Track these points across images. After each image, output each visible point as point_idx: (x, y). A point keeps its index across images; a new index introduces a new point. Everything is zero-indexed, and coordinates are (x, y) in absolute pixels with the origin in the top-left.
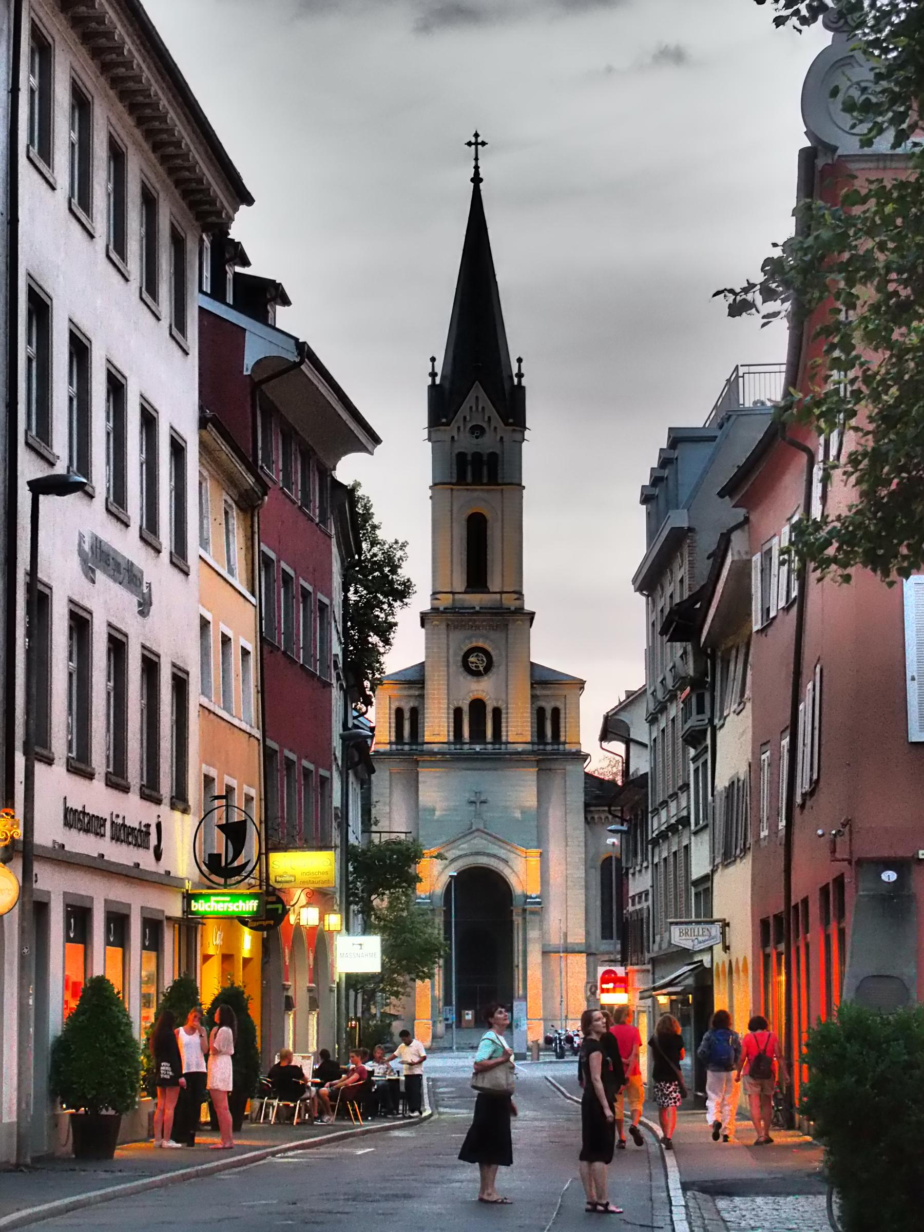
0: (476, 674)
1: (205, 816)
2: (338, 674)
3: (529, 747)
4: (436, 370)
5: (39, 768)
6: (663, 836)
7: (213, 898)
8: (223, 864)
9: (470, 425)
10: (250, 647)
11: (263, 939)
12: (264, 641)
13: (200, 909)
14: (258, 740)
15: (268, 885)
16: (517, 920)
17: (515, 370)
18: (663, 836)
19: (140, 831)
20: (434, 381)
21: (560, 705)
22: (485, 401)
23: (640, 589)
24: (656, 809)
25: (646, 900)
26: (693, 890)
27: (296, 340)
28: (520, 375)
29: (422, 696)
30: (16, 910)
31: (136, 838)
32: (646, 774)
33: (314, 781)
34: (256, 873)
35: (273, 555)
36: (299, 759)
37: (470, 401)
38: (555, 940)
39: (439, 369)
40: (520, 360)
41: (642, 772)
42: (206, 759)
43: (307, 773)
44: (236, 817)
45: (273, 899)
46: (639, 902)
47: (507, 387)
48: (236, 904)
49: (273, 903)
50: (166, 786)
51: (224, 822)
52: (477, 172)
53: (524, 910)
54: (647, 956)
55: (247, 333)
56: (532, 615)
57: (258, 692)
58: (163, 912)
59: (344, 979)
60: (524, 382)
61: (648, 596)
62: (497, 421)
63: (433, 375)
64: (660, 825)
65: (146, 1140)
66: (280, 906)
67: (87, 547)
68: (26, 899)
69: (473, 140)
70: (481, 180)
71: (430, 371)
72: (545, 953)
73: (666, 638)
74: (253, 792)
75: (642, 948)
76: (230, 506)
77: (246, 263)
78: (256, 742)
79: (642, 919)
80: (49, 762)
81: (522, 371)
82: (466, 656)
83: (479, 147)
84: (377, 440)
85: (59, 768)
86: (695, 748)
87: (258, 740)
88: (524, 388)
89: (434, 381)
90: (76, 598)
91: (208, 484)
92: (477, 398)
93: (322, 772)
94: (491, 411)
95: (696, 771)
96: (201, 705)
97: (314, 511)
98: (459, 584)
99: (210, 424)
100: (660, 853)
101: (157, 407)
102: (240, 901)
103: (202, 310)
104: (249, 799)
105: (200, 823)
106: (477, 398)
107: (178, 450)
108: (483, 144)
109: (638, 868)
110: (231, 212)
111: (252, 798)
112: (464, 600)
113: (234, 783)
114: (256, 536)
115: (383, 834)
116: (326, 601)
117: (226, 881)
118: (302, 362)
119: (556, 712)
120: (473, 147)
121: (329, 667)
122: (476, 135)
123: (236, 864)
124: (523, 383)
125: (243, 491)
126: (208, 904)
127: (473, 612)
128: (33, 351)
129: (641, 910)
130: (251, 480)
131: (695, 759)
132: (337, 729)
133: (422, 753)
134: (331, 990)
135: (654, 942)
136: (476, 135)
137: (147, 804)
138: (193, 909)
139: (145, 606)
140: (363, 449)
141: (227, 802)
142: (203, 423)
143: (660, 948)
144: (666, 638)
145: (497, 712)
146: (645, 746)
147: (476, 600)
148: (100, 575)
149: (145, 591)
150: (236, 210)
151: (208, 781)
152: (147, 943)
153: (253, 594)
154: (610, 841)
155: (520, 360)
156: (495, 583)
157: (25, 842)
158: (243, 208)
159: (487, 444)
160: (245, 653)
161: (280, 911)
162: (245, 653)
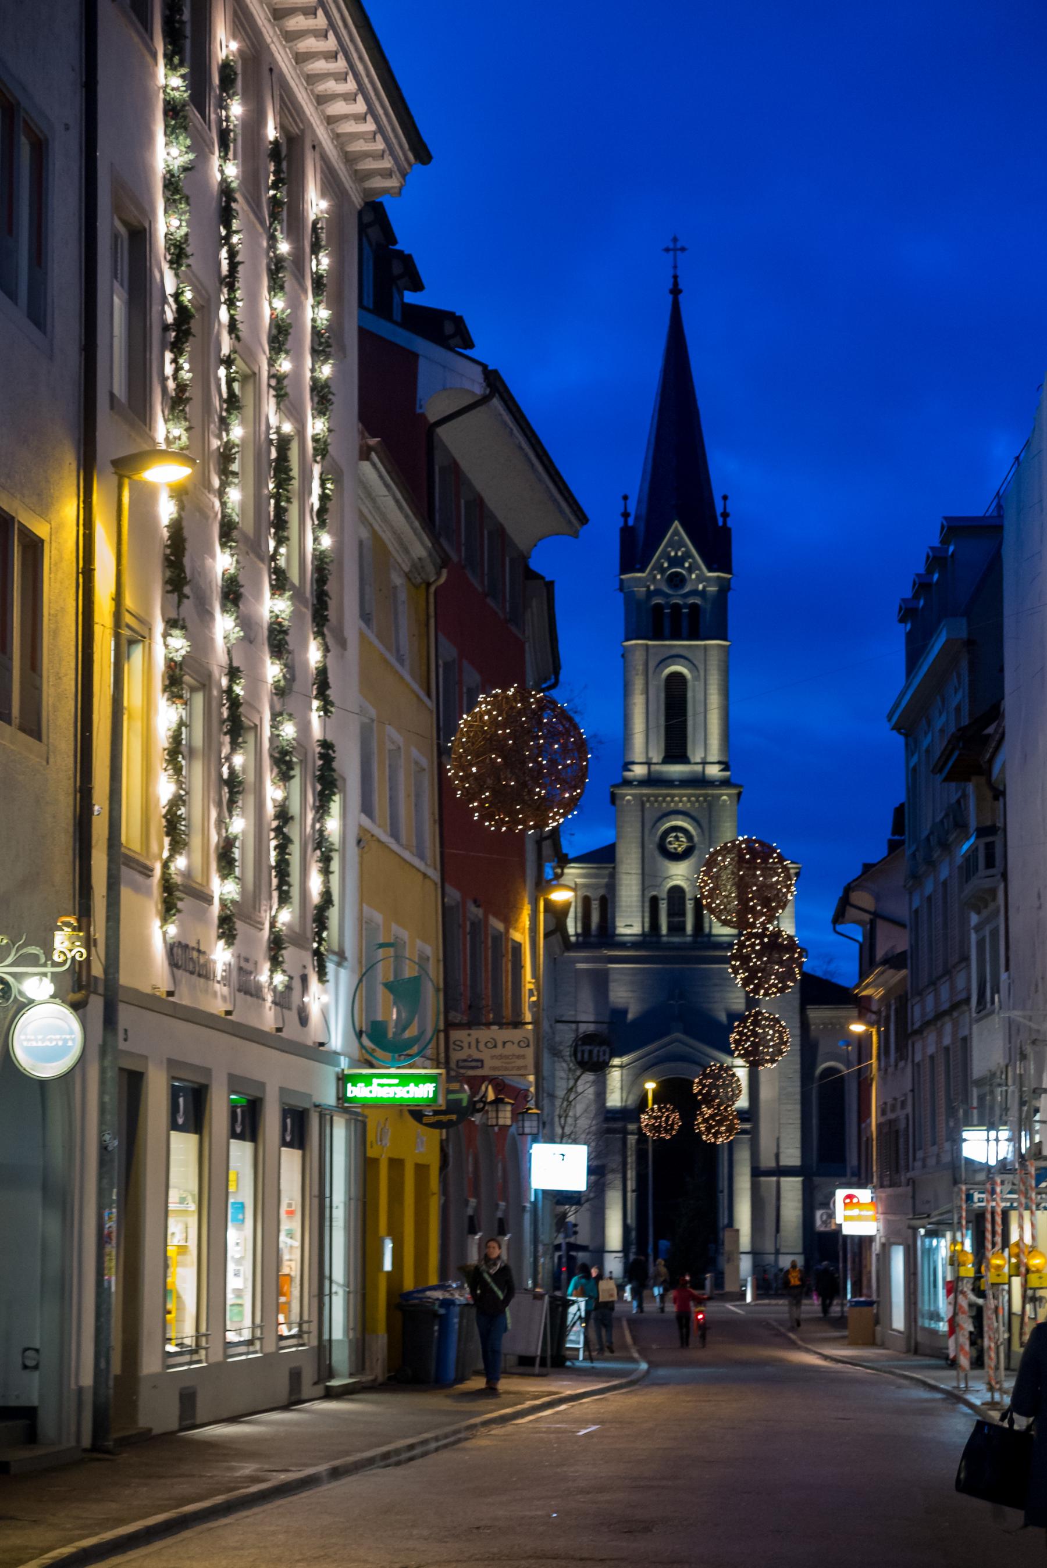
1: (367, 971)
4: (629, 510)
7: (375, 1081)
11: (442, 1141)
13: (359, 1096)
14: (436, 884)
17: (719, 509)
20: (626, 521)
23: (897, 728)
27: (484, 367)
28: (725, 515)
32: (904, 953)
38: (767, 1161)
39: (632, 508)
40: (725, 498)
41: (899, 950)
48: (407, 1088)
51: (392, 979)
52: (676, 283)
55: (422, 362)
57: (435, 821)
58: (310, 1096)
59: (540, 1196)
60: (730, 523)
61: (906, 736)
63: (626, 515)
65: (286, 1407)
68: (107, 1063)
69: (671, 246)
70: (680, 291)
71: (622, 510)
72: (757, 1172)
73: (940, 778)
77: (417, 286)
79: (897, 1132)
81: (728, 510)
83: (679, 253)
86: (979, 913)
87: (436, 884)
88: (729, 530)
89: (626, 521)
95: (981, 944)
100: (924, 1048)
102: (412, 1085)
105: (360, 981)
108: (683, 249)
111: (428, 959)
112: (661, 773)
114: (432, 621)
115: (581, 1025)
120: (671, 253)
122: (675, 240)
124: (729, 524)
125: (416, 560)
126: (369, 1088)
131: (978, 928)
135: (914, 1159)
136: (675, 240)
138: (349, 1095)
141: (396, 952)
144: (940, 778)
152: (288, 1139)
153: (429, 695)
155: (725, 498)
157: (106, 980)
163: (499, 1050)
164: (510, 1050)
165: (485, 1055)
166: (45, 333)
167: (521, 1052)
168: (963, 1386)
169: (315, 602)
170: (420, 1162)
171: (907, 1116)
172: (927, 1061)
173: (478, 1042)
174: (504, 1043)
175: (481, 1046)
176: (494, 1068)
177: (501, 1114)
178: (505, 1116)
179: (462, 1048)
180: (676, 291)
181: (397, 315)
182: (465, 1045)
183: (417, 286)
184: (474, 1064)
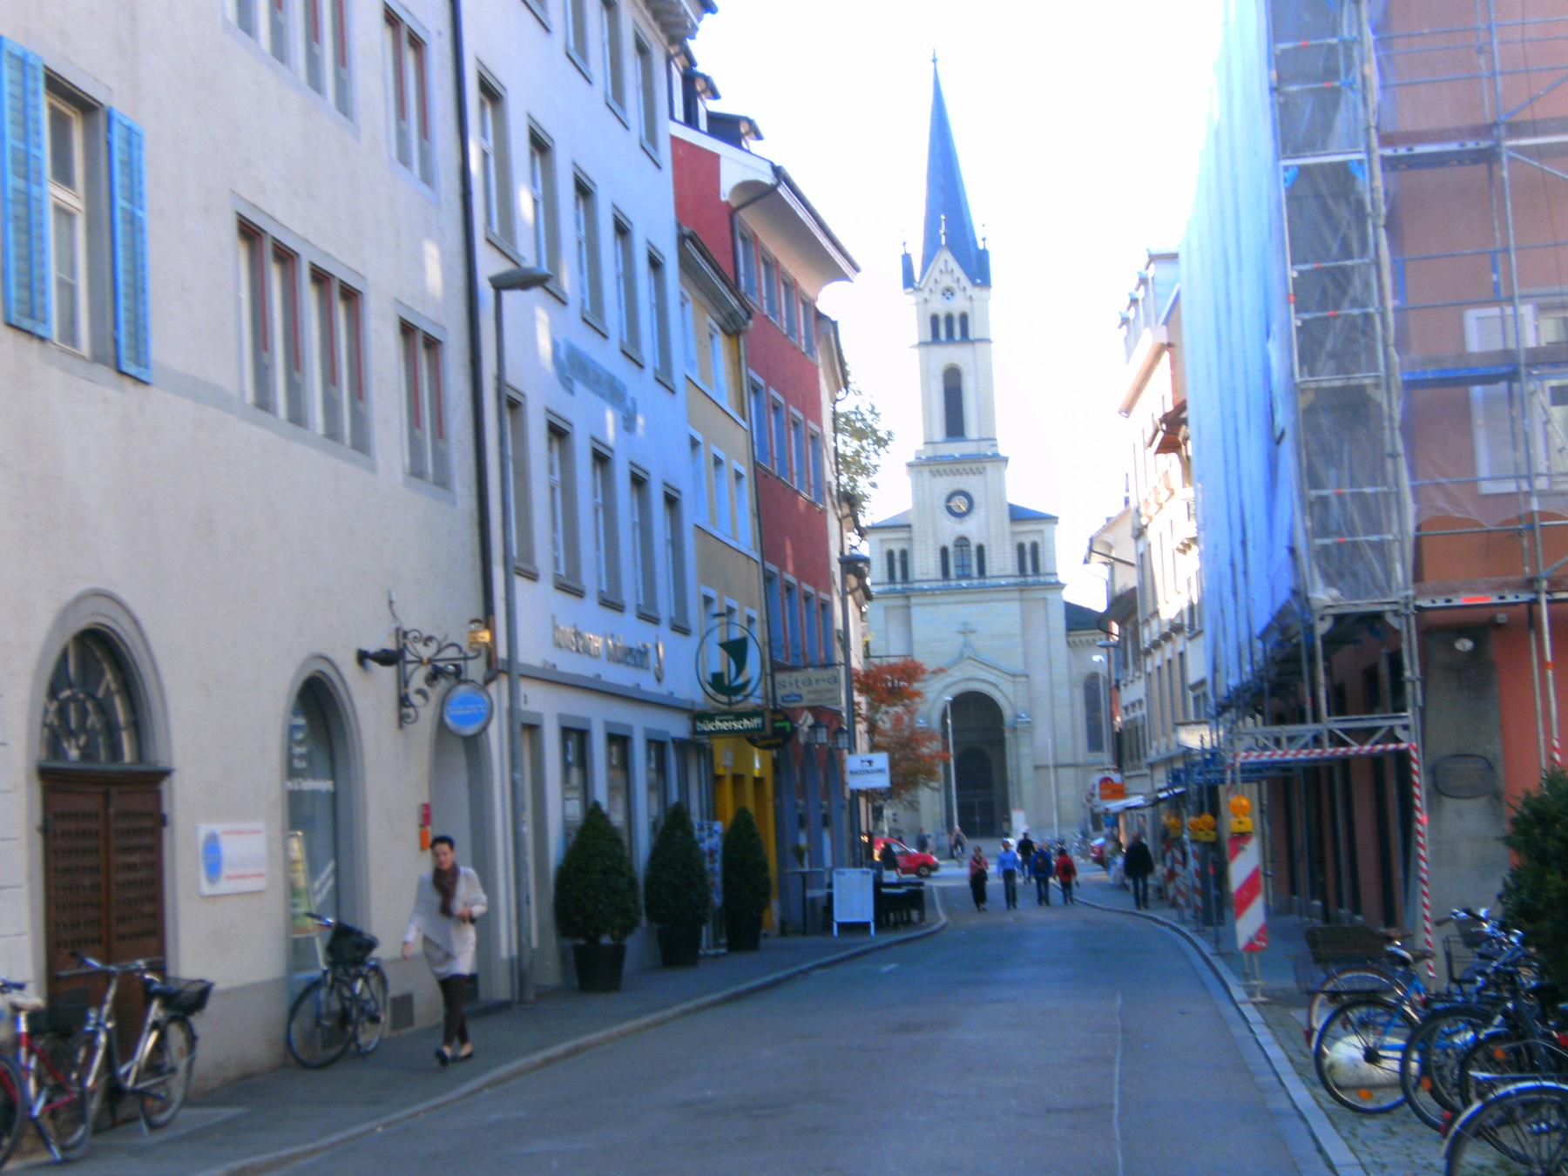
0: (960, 515)
2: (833, 503)
3: (1012, 580)
5: (520, 583)
6: (1156, 645)
8: (726, 682)
9: (941, 287)
10: (743, 470)
12: (756, 466)
15: (775, 703)
16: (1008, 735)
18: (1156, 645)
19: (639, 651)
21: (1037, 538)
22: (953, 264)
24: (1147, 621)
25: (1140, 708)
26: (1191, 694)
27: (772, 164)
29: (910, 540)
30: (1228, 857)
31: (635, 658)
33: (815, 605)
34: (758, 693)
35: (761, 381)
36: (799, 583)
37: (941, 265)
40: (984, 240)
42: (706, 579)
43: (807, 598)
44: (737, 634)
45: (780, 717)
46: (1133, 711)
47: (973, 251)
49: (781, 721)
50: (665, 608)
53: (1015, 729)
54: (1144, 761)
56: (1005, 460)
62: (965, 281)
64: (1151, 634)
66: (787, 724)
67: (562, 355)
74: (755, 614)
75: (1137, 754)
76: (715, 331)
77: (715, 95)
78: (754, 563)
79: (1137, 728)
80: (533, 577)
82: (950, 498)
84: (857, 269)
85: (545, 586)
90: (554, 408)
91: (689, 307)
92: (946, 261)
93: (823, 596)
94: (959, 273)
96: (696, 526)
97: (800, 340)
98: (939, 432)
99: (688, 241)
101: (631, 219)
103: (675, 141)
104: (750, 620)
106: (946, 261)
107: (655, 264)
109: (1130, 678)
110: (695, 20)
113: (734, 604)
116: (817, 429)
117: (730, 699)
118: (779, 184)
119: (1035, 546)
121: (823, 494)
123: (740, 681)
127: (954, 460)
128: (490, 144)
129: (1135, 719)
130: (734, 302)
132: (835, 554)
133: (913, 590)
134: (843, 807)
137: (644, 624)
139: (628, 423)
140: (844, 277)
142: (682, 239)
143: (1158, 752)
145: (980, 549)
146: (1131, 565)
147: (956, 449)
148: (579, 387)
149: (630, 405)
150: (700, 19)
151: (708, 601)
153: (744, 419)
154: (1096, 658)
155: (984, 240)
156: (972, 430)
158: (708, 16)
159: (957, 305)
160: (739, 476)
161: (788, 729)
162: (739, 476)
163: (815, 687)
164: (823, 686)
165: (803, 691)
166: (352, 121)
167: (831, 686)
168: (905, 918)
169: (658, 366)
170: (565, 725)
171: (1143, 717)
172: (1156, 671)
173: (797, 681)
174: (817, 681)
175: (800, 685)
176: (810, 701)
177: (819, 735)
178: (822, 737)
179: (784, 686)
180: (934, 61)
181: (703, 123)
182: (787, 684)
183: (715, 95)
184: (795, 698)
